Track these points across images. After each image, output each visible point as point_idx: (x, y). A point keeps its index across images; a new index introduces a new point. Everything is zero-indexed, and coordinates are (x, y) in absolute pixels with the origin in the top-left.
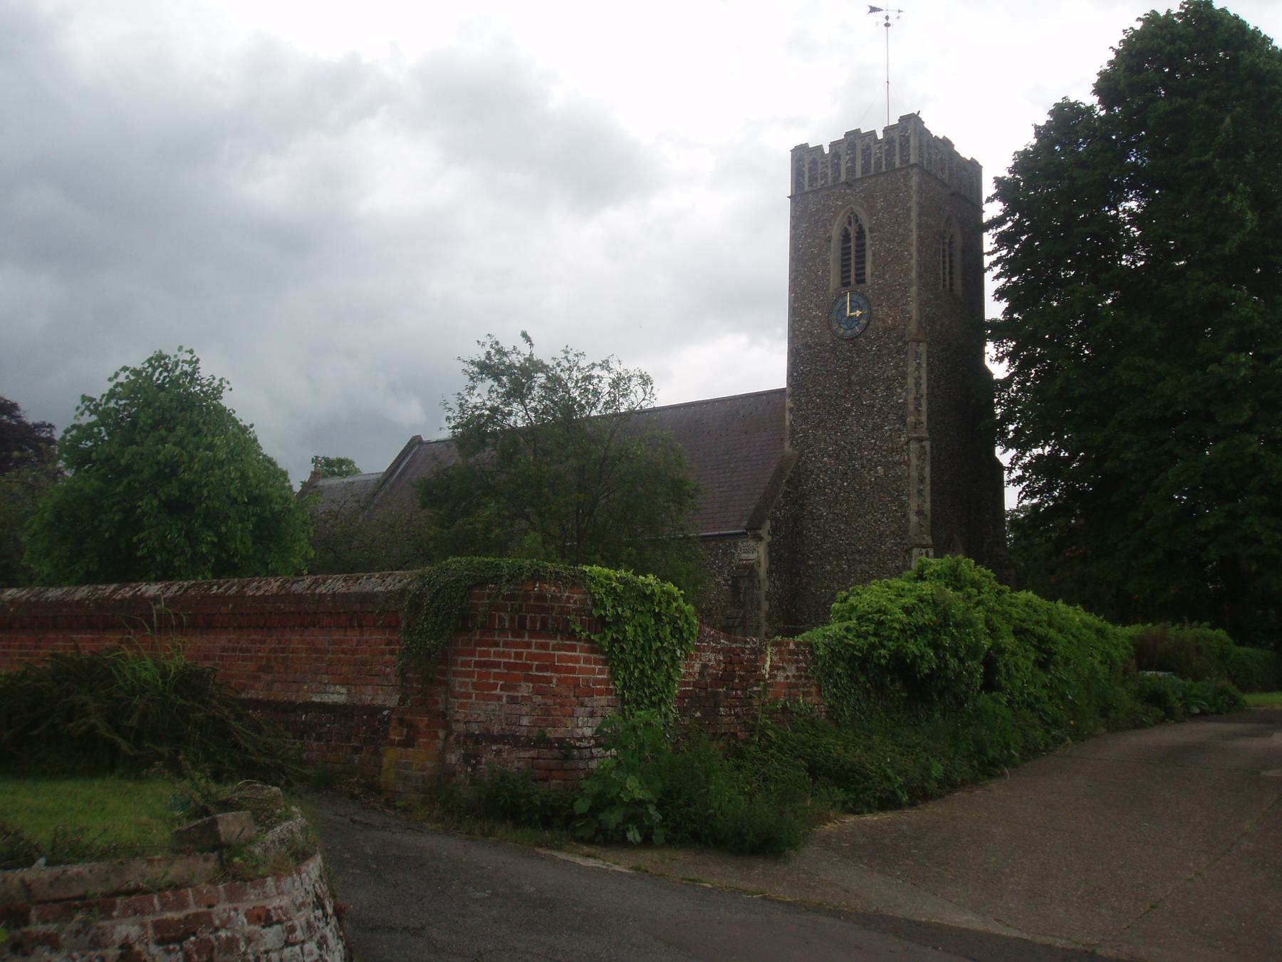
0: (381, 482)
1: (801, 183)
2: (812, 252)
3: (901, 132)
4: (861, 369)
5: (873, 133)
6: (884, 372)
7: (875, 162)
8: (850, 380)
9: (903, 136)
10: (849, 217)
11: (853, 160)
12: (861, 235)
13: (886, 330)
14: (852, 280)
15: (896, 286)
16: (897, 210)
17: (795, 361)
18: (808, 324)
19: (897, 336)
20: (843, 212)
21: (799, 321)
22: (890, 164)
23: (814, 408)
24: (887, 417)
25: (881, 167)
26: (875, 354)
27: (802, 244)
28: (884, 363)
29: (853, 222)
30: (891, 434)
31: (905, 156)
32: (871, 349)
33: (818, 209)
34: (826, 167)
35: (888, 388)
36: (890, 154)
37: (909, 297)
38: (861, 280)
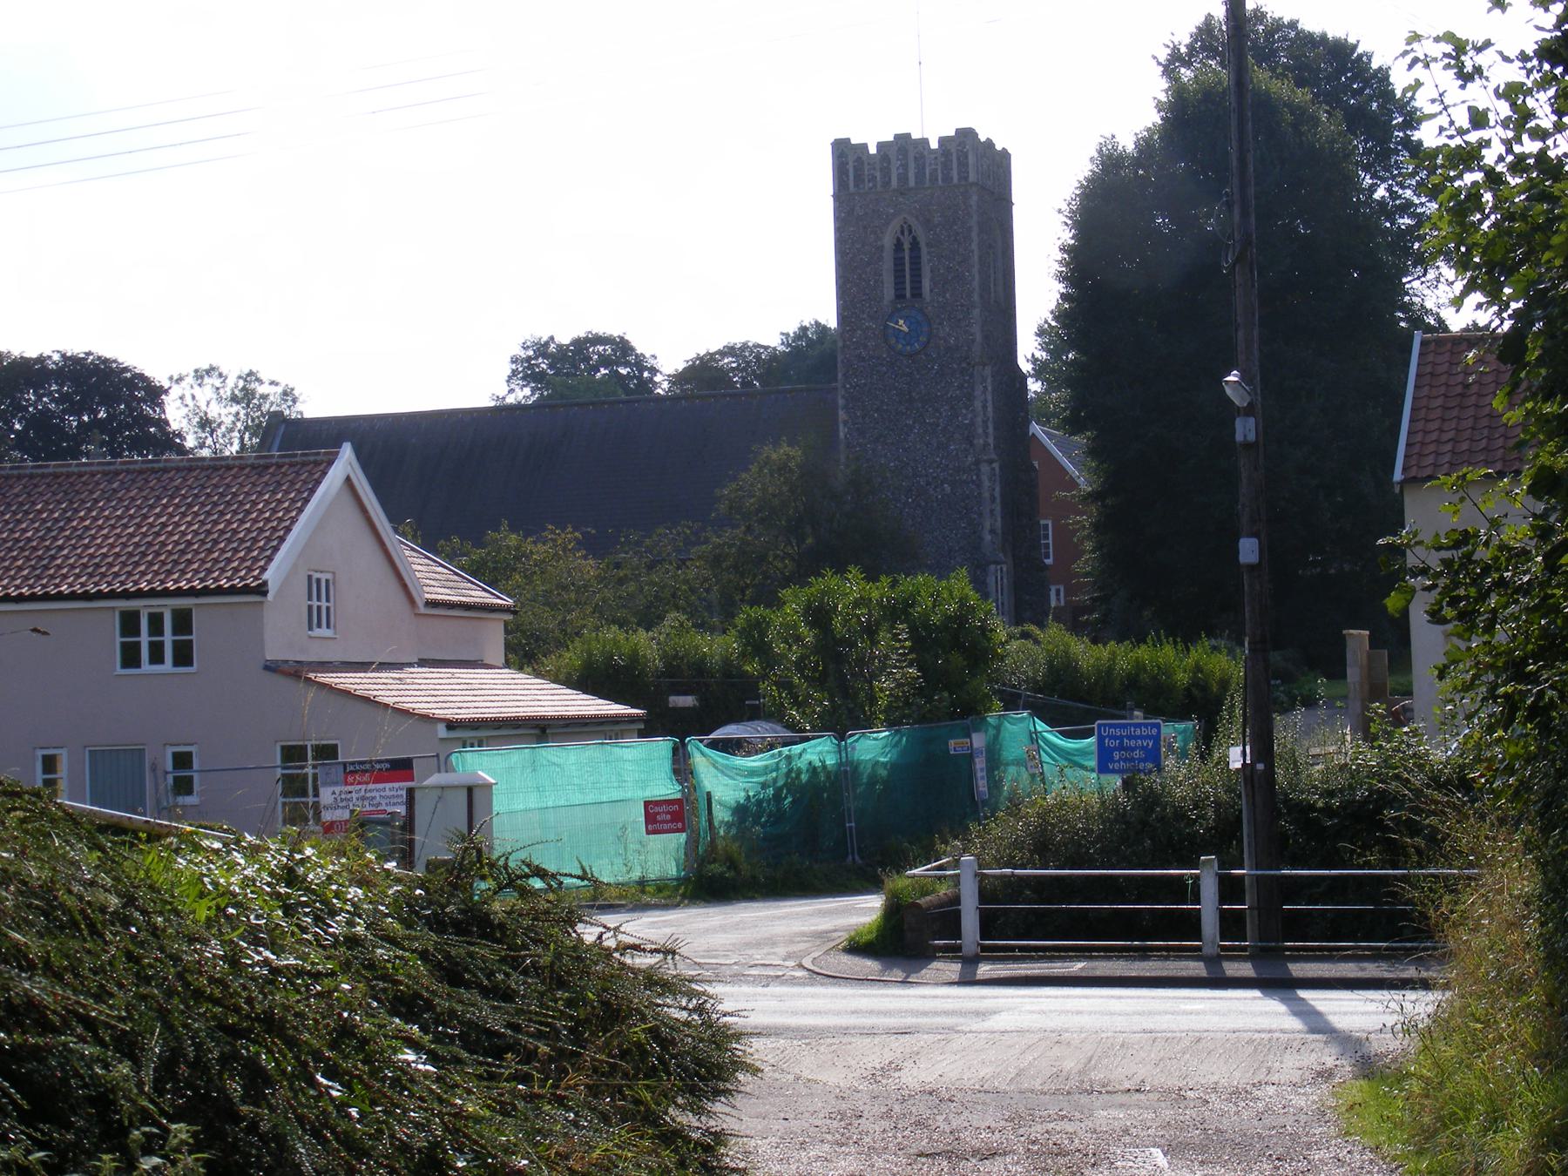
3: (959, 145)
4: (922, 387)
7: (930, 174)
10: (902, 227)
12: (915, 245)
25: (937, 180)
29: (906, 233)
38: (917, 293)
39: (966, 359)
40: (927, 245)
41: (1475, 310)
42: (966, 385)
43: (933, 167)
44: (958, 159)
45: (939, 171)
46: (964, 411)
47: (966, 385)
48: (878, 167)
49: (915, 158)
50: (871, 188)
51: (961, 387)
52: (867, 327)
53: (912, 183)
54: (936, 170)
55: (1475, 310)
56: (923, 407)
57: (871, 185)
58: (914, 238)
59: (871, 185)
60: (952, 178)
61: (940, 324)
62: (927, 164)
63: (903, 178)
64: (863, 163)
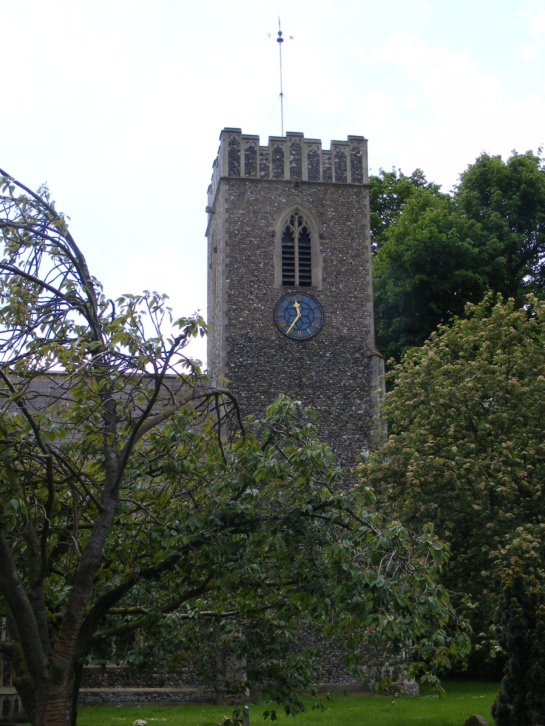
0: (136, 436)
1: (235, 167)
2: (251, 241)
3: (353, 150)
4: (313, 373)
5: (256, 139)
6: (341, 380)
7: (324, 171)
8: (301, 381)
9: (355, 155)
10: (292, 217)
11: (298, 161)
12: (305, 236)
13: (341, 339)
14: (297, 280)
15: (350, 297)
16: (349, 223)
17: (232, 351)
18: (247, 315)
19: (355, 347)
20: (288, 210)
21: (236, 309)
22: (341, 177)
23: (257, 404)
24: (345, 426)
25: (331, 178)
26: (329, 361)
27: (239, 230)
28: (340, 371)
29: (296, 223)
30: (350, 443)
31: (358, 175)
32: (324, 354)
33: (256, 200)
34: (267, 160)
35: (345, 397)
36: (341, 168)
37: (366, 311)
38: (306, 281)
39: (360, 349)
40: (321, 237)
41: (440, 186)
42: (360, 375)
43: (327, 165)
44: (352, 162)
45: (333, 169)
46: (358, 401)
47: (360, 375)
48: (270, 158)
49: (309, 155)
50: (263, 177)
51: (354, 377)
52: (255, 309)
53: (305, 177)
54: (330, 169)
55: (440, 186)
56: (314, 394)
57: (263, 173)
58: (305, 229)
59: (263, 173)
60: (346, 178)
61: (332, 313)
62: (321, 163)
63: (295, 171)
64: (255, 152)
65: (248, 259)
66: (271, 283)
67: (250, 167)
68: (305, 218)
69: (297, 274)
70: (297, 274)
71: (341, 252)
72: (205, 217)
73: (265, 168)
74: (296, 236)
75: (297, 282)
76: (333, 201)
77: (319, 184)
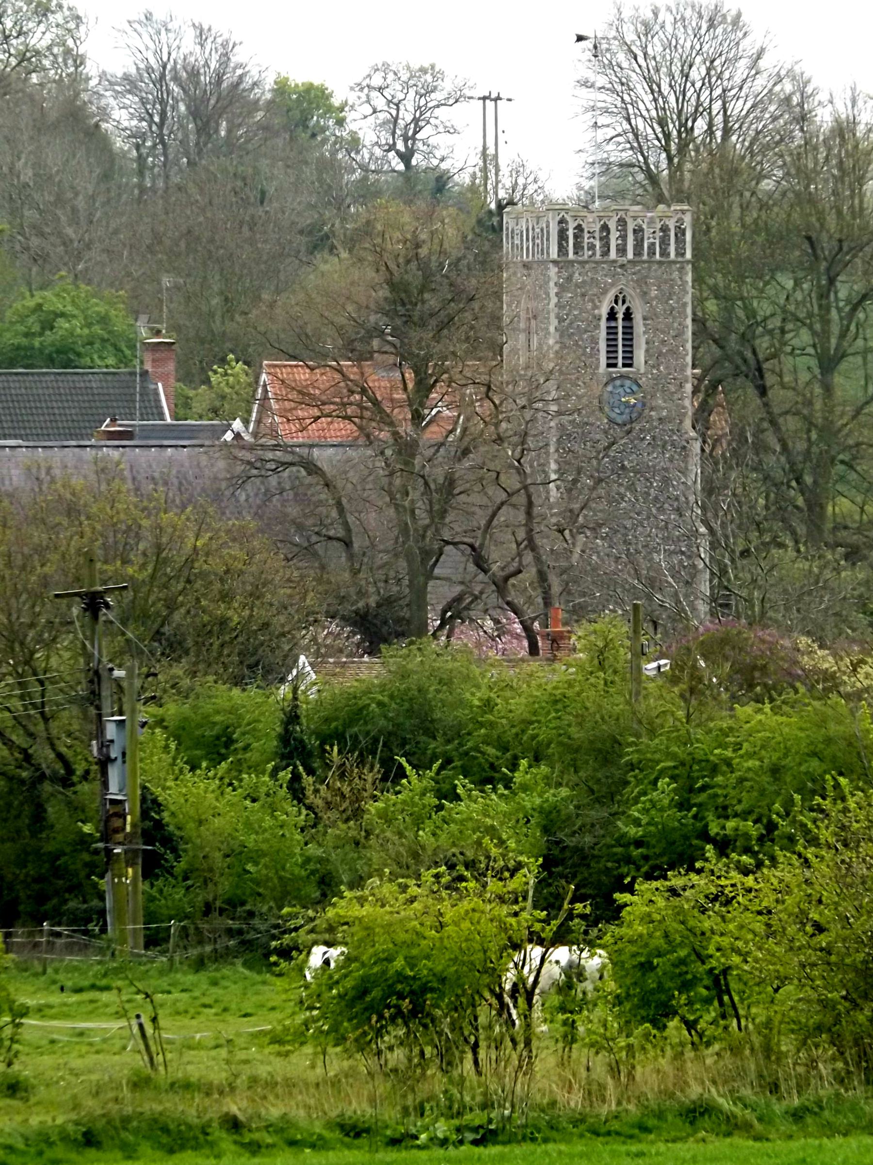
11: (624, 237)
12: (628, 316)
14: (620, 362)
33: (584, 282)
48: (597, 235)
54: (653, 244)
65: (576, 344)
66: (597, 367)
67: (578, 247)
68: (628, 298)
69: (620, 355)
70: (620, 355)
71: (663, 332)
72: (178, 1157)
73: (592, 247)
74: (620, 316)
75: (620, 364)
76: (656, 278)
77: (644, 262)
